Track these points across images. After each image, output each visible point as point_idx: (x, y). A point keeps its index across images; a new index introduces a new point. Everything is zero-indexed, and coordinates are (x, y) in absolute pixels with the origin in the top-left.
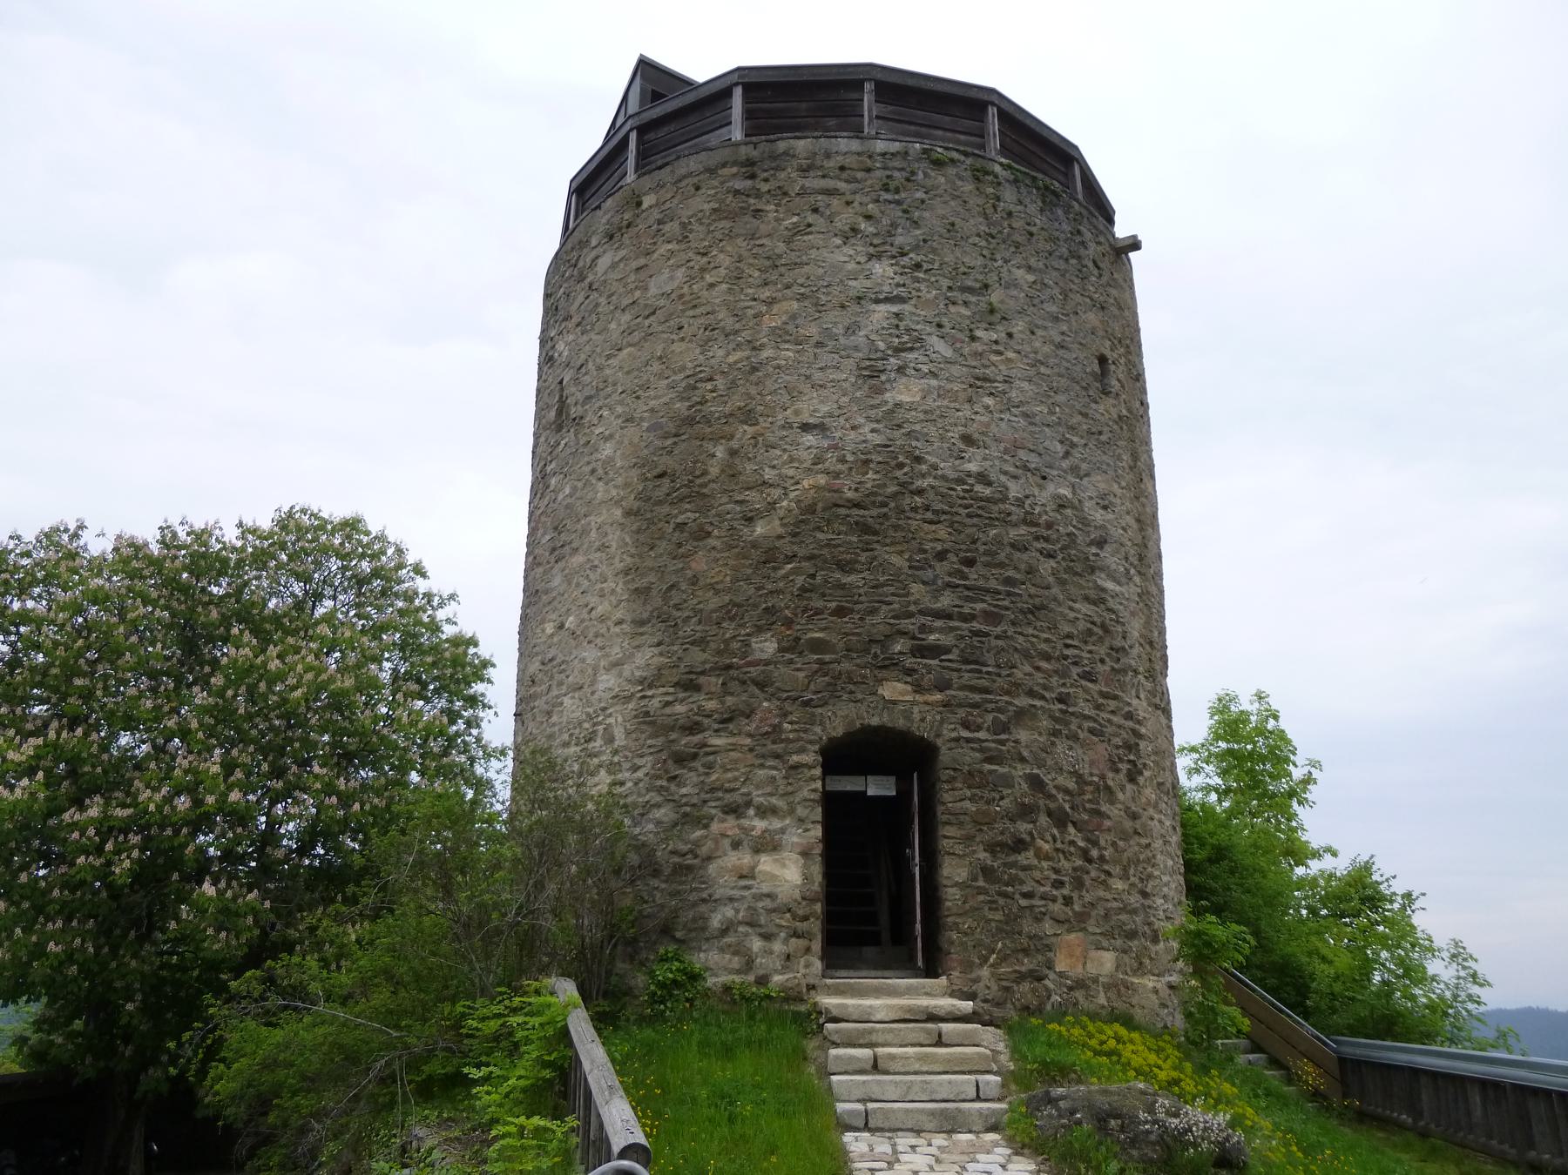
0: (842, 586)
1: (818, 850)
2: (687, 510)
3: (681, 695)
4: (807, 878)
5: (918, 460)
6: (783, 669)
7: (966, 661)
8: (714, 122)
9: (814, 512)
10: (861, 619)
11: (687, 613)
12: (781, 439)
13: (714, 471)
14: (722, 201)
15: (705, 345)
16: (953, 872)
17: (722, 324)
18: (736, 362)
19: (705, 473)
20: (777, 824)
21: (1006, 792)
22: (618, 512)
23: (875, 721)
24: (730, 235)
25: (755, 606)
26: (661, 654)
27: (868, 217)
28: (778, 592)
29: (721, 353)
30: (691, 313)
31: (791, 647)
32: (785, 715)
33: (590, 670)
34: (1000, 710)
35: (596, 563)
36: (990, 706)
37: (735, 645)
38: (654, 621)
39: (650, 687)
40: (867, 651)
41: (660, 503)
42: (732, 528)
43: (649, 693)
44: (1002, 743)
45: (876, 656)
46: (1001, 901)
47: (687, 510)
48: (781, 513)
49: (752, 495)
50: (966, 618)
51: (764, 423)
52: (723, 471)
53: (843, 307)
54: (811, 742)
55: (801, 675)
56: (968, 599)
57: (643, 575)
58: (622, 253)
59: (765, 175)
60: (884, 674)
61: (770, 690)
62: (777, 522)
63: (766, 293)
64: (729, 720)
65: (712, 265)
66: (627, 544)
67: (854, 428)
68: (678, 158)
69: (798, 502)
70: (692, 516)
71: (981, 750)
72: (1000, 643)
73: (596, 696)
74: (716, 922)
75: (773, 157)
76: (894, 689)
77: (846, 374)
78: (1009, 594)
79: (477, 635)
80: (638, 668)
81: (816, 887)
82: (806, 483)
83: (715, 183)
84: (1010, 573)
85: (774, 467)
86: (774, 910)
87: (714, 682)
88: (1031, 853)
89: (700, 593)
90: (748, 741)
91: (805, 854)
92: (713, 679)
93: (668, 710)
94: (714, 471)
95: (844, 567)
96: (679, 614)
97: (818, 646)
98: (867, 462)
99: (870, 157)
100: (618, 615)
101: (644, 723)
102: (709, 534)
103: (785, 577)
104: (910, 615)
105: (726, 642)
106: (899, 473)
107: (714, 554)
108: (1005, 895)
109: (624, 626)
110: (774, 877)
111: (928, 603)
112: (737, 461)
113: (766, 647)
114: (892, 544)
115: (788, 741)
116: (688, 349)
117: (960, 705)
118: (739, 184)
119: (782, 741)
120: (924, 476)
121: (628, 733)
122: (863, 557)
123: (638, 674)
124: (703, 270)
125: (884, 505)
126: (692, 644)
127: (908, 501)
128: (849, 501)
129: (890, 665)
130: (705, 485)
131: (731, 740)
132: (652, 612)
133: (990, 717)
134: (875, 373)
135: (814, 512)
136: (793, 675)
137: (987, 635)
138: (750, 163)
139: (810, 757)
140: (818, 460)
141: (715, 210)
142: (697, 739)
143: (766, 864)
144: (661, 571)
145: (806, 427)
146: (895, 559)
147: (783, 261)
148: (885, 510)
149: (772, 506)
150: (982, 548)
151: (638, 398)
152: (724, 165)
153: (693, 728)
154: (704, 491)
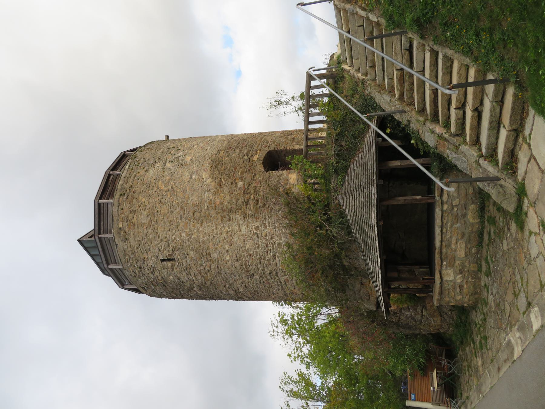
2: (204, 206)
7: (252, 147)
10: (238, 164)
15: (164, 204)
21: (281, 141)
27: (144, 168)
30: (154, 208)
31: (241, 179)
34: (264, 142)
35: (212, 237)
44: (271, 142)
47: (204, 206)
50: (242, 148)
53: (164, 172)
56: (238, 148)
60: (251, 161)
63: (155, 189)
65: (144, 203)
67: (194, 168)
70: (206, 205)
72: (249, 143)
73: (247, 234)
76: (255, 158)
77: (180, 170)
91: (289, 173)
92: (246, 197)
96: (229, 207)
113: (240, 184)
117: (261, 148)
118: (125, 197)
123: (242, 219)
132: (228, 215)
134: (182, 165)
145: (191, 178)
153: (257, 201)
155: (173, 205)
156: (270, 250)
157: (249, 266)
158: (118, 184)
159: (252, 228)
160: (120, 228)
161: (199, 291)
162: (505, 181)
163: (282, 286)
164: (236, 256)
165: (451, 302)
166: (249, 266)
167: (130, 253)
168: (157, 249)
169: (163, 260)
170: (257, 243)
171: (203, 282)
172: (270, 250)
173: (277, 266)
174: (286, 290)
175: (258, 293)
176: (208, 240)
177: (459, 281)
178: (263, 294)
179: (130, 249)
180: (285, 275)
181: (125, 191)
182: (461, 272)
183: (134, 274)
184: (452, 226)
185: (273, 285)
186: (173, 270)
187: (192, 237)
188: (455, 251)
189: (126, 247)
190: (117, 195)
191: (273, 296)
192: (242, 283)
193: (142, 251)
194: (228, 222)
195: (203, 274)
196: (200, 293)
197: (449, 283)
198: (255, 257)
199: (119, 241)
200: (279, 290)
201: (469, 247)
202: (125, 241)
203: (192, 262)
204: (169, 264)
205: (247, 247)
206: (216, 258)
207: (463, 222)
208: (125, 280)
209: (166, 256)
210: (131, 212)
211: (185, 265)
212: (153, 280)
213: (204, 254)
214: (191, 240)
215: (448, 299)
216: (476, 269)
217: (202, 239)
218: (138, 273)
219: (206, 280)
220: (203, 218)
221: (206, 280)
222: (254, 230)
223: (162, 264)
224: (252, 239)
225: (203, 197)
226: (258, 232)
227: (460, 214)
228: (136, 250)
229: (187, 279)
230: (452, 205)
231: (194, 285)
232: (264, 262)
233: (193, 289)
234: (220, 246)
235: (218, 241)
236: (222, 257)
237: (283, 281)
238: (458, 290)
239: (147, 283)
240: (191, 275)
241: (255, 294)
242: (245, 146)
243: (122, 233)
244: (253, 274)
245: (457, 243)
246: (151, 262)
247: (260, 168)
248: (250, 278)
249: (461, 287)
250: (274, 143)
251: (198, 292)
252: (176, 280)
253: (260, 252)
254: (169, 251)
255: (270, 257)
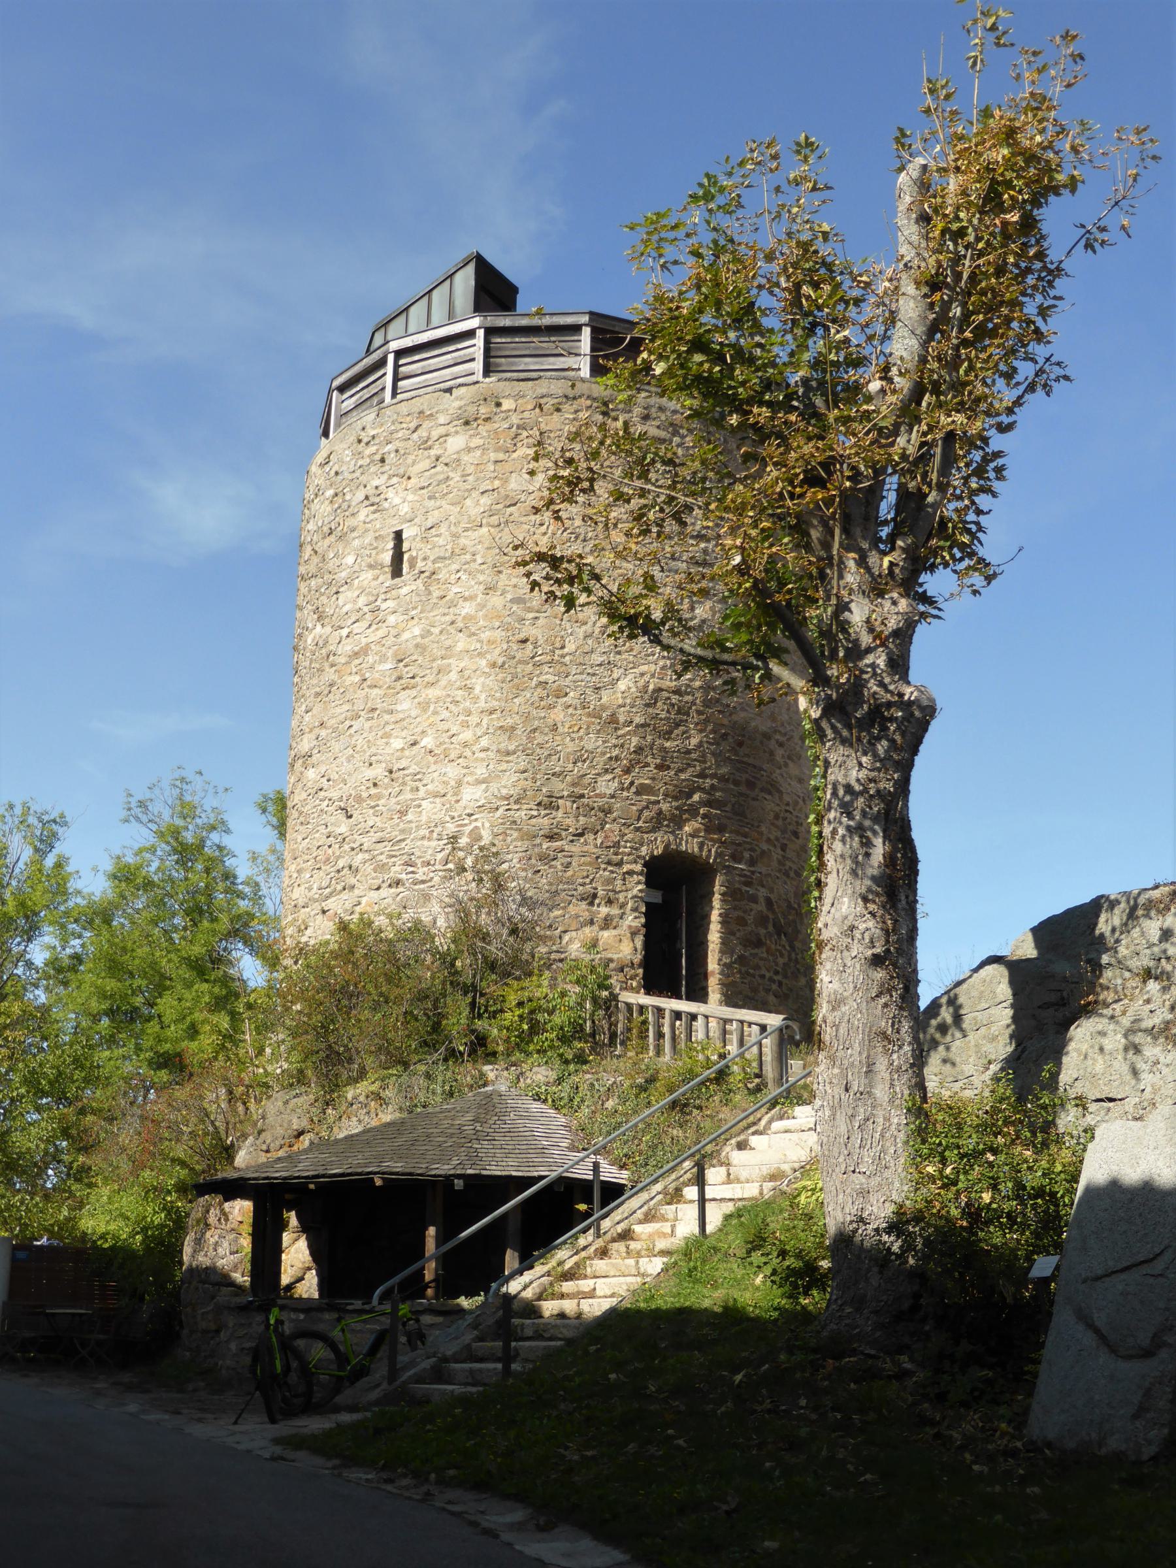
3: (543, 812)
35: (458, 699)
38: (519, 753)
47: (547, 673)
58: (477, 441)
64: (581, 835)
88: (764, 950)
100: (484, 742)
109: (489, 753)
123: (504, 792)
137: (747, 796)
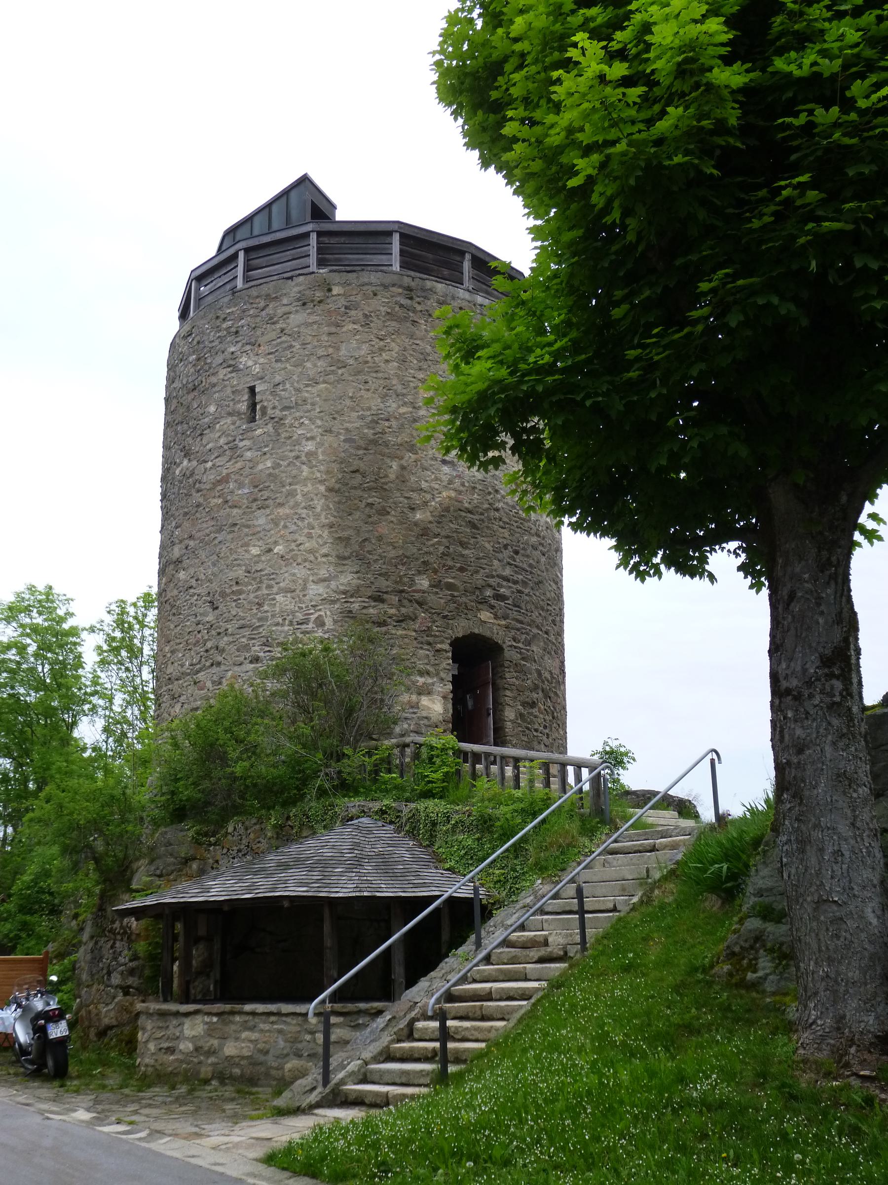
0: (463, 556)
1: (451, 696)
3: (373, 604)
4: (445, 710)
5: (497, 491)
6: (433, 597)
7: (515, 606)
8: (376, 249)
9: (448, 512)
10: (472, 575)
11: (376, 557)
12: (431, 465)
13: (392, 476)
14: (393, 309)
15: (384, 397)
16: (510, 714)
17: (395, 387)
18: (404, 414)
19: (386, 476)
20: (430, 681)
21: (529, 676)
22: (322, 488)
23: (476, 631)
24: (397, 332)
25: (417, 559)
26: (359, 578)
28: (430, 553)
29: (394, 405)
30: (375, 375)
31: (436, 585)
32: (434, 622)
33: (300, 581)
34: (527, 634)
35: (304, 516)
36: (524, 631)
37: (405, 580)
39: (352, 596)
40: (474, 593)
41: (355, 488)
42: (403, 512)
43: (352, 600)
44: (528, 650)
45: (478, 597)
46: (527, 732)
48: (431, 509)
49: (414, 495)
50: (516, 582)
51: (421, 454)
52: (397, 478)
54: (446, 638)
55: (442, 601)
56: (516, 572)
57: (343, 530)
59: (418, 299)
60: (480, 606)
61: (425, 607)
62: (429, 514)
63: (421, 375)
65: (387, 348)
66: (330, 509)
68: (363, 270)
69: (440, 504)
70: (377, 500)
71: (521, 653)
72: (527, 598)
73: (307, 597)
74: (397, 730)
75: (423, 290)
76: (485, 615)
78: (531, 573)
79: (698, 584)
80: (342, 584)
81: (450, 715)
82: (444, 494)
83: (387, 295)
84: (531, 561)
85: (426, 481)
86: (429, 726)
87: (395, 599)
89: (384, 546)
90: (414, 634)
91: (444, 697)
92: (393, 597)
93: (364, 611)
94: (392, 476)
95: (463, 544)
96: (371, 557)
97: (450, 587)
98: (474, 488)
99: (474, 305)
100: (324, 550)
101: (348, 617)
102: (388, 513)
103: (433, 545)
104: (493, 577)
105: (401, 577)
106: (489, 497)
107: (391, 525)
108: (528, 728)
110: (429, 708)
111: (500, 572)
112: (405, 473)
113: (424, 583)
114: (486, 536)
115: (436, 636)
116: (373, 398)
117: (513, 628)
118: (404, 301)
119: (432, 636)
120: (499, 501)
121: (335, 622)
122: (472, 541)
123: (342, 588)
124: (381, 349)
125: (482, 514)
126: (380, 575)
127: (492, 514)
128: (466, 508)
129: (483, 602)
130: (386, 484)
131: (404, 632)
132: (351, 553)
133: (524, 636)
135: (448, 512)
136: (438, 600)
138: (409, 289)
139: (446, 646)
140: (450, 482)
141: (388, 313)
142: (384, 629)
143: (425, 701)
144: (358, 531)
146: (487, 545)
147: (430, 358)
148: (482, 517)
149: (426, 503)
150: (522, 546)
151: (334, 418)
152: (394, 285)
153: (381, 624)
154: (385, 487)
155: (380, 421)
156: (269, 651)
157: (235, 601)
158: (436, 281)
159: (320, 610)
160: (330, 290)
161: (181, 472)
162: (320, 1093)
163: (189, 674)
164: (257, 571)
165: (143, 1034)
166: (235, 601)
167: (269, 310)
168: (278, 379)
169: (252, 390)
170: (287, 622)
171: (203, 486)
172: (269, 651)
173: (235, 665)
174: (180, 682)
175: (174, 614)
176: (297, 504)
177: (182, 1047)
178: (172, 626)
179: (280, 311)
180: (213, 682)
181: (418, 299)
182: (197, 1049)
183: (223, 316)
184: (280, 1031)
185: (192, 653)
186: (230, 414)
187: (304, 467)
188: (237, 1039)
189: (285, 301)
190: (410, 279)
191: (167, 649)
192: (197, 580)
193: (274, 342)
194: (334, 554)
195: (219, 488)
196: (177, 472)
197: (179, 1028)
198: (256, 614)
199: (301, 285)
200: (182, 666)
201: (242, 1063)
202: (299, 300)
203: (249, 464)
204: (243, 407)
205: (277, 597)
206: (256, 523)
207: (285, 1052)
208: (208, 287)
209: (262, 401)
210: (366, 316)
211: (241, 444)
212: (209, 361)
213: (266, 494)
214: (298, 464)
215: (149, 1027)
216: (202, 1076)
217: (299, 491)
218: (224, 326)
219: (204, 492)
220: (347, 494)
221: (204, 492)
222: (316, 615)
223: (243, 389)
224: (297, 608)
225: (398, 494)
226: (311, 625)
227: (300, 1046)
228: (278, 326)
229: (208, 447)
230: (315, 1032)
231: (195, 463)
232: (244, 637)
233: (185, 456)
234: (282, 532)
235: (294, 528)
236: (257, 536)
237: (201, 676)
238: (166, 1045)
239: (201, 346)
240: (217, 457)
241: (173, 606)
242: (520, 588)
243: (319, 294)
244: (217, 608)
245: (251, 1041)
246: (250, 363)
247: (461, 627)
248: (209, 599)
249: (171, 1050)
250: (523, 659)
251: (180, 469)
252: (206, 420)
253: (265, 627)
254: (274, 408)
255: (255, 651)
